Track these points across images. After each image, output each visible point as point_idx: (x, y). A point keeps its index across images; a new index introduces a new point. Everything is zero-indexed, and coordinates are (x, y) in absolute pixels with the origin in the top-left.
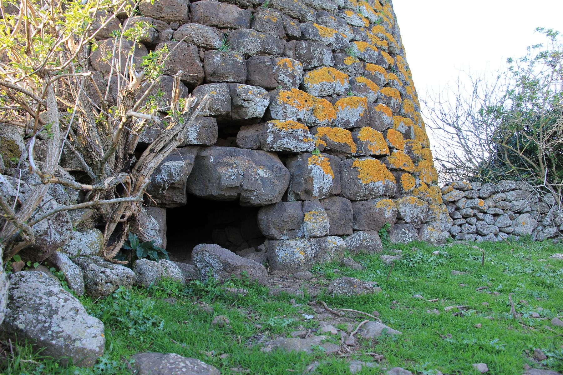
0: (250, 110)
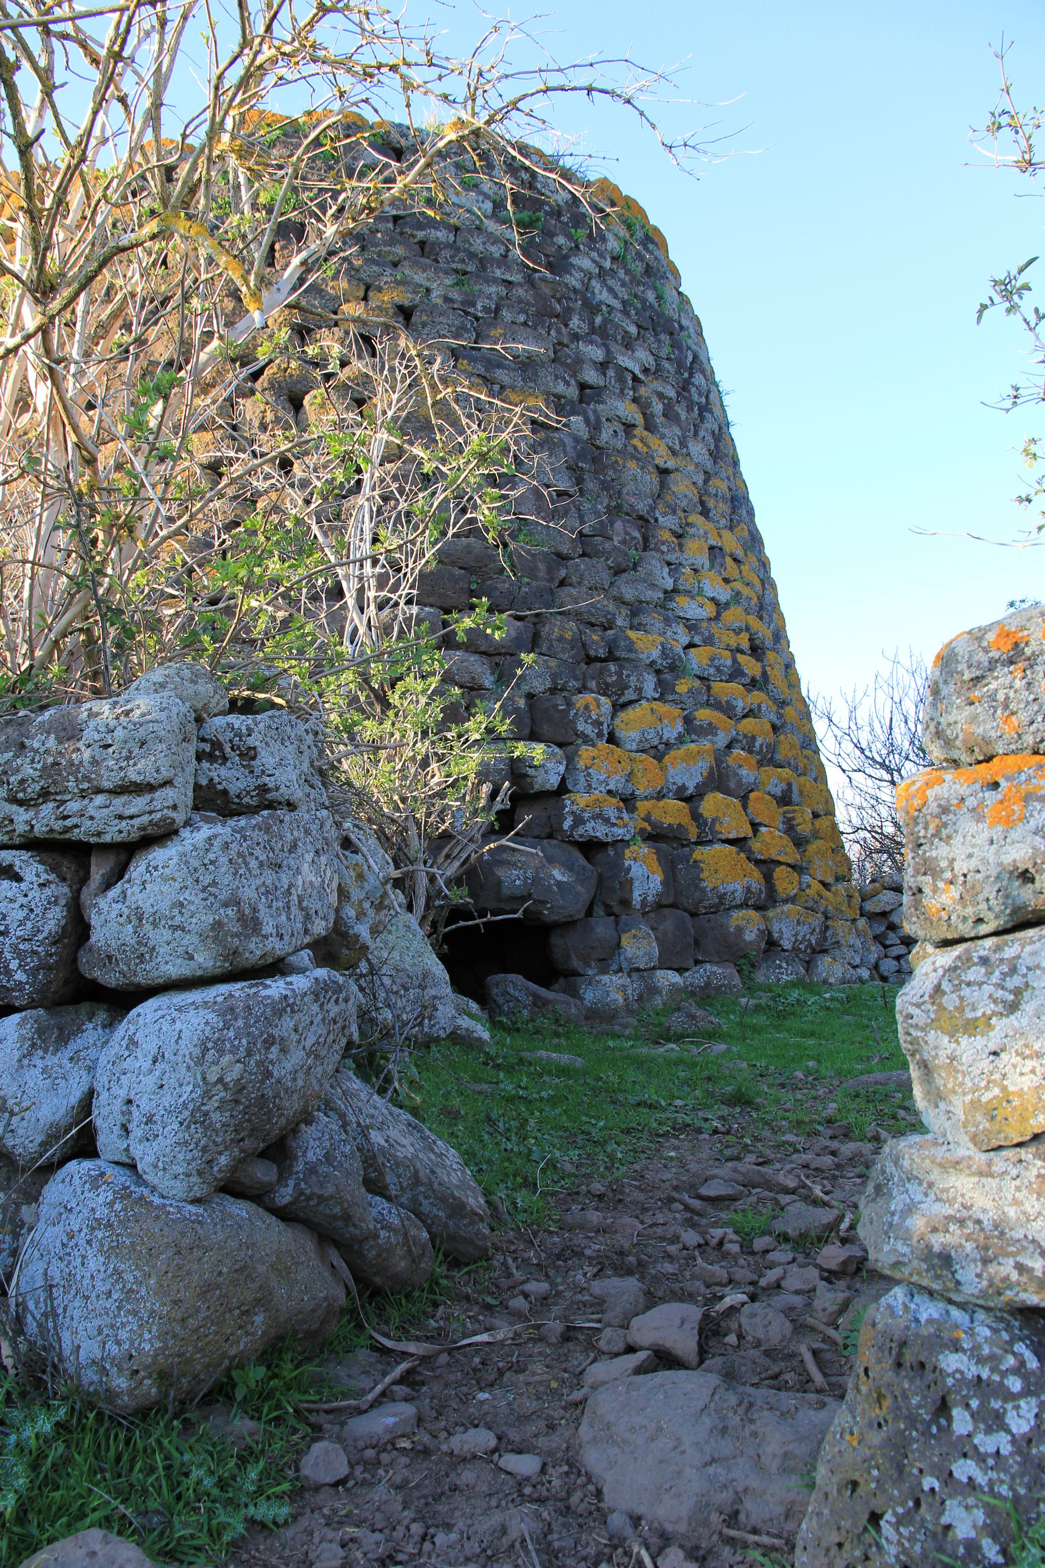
0: (539, 780)
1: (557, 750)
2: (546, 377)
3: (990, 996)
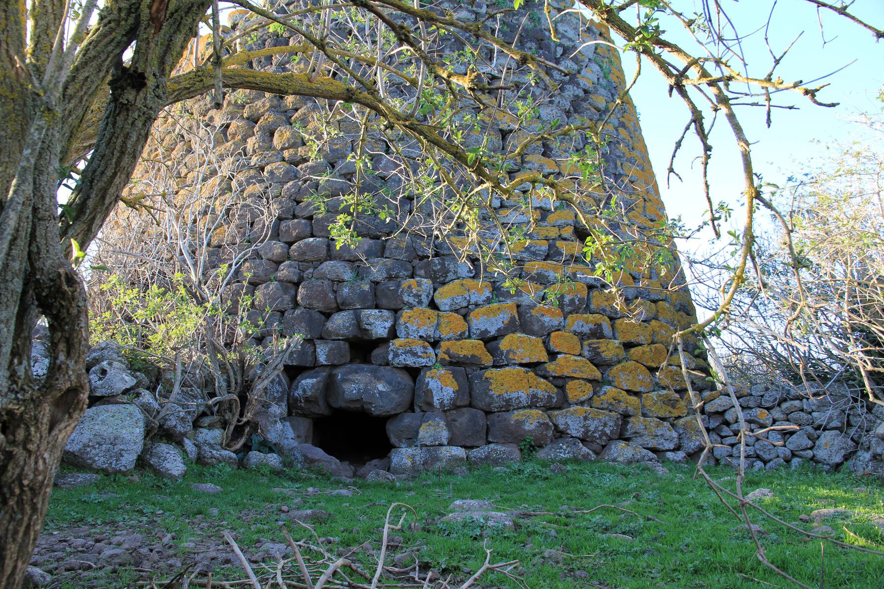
0: (374, 332)
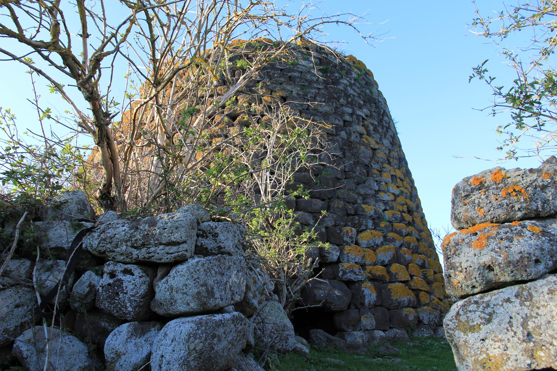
0: (330, 258)
1: (336, 247)
2: (332, 118)
3: (479, 316)
